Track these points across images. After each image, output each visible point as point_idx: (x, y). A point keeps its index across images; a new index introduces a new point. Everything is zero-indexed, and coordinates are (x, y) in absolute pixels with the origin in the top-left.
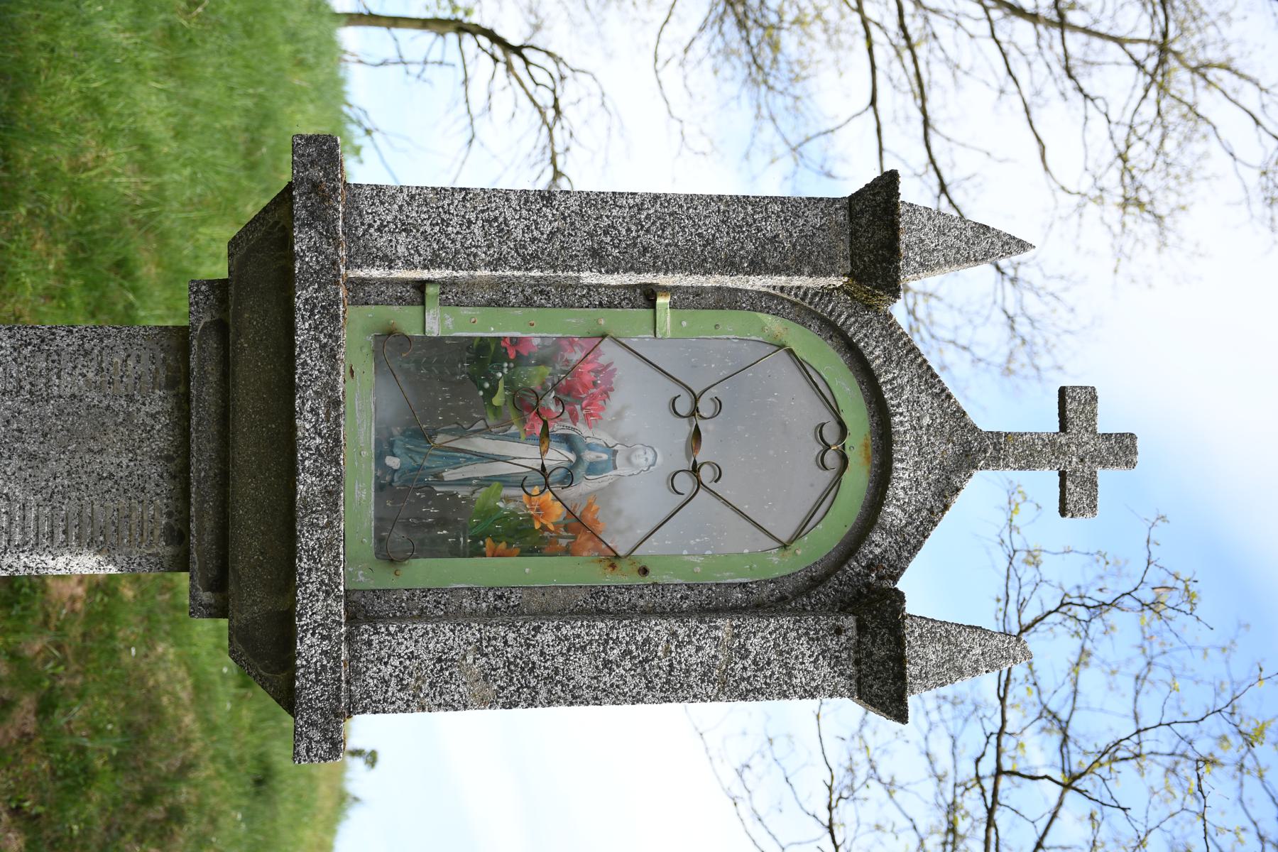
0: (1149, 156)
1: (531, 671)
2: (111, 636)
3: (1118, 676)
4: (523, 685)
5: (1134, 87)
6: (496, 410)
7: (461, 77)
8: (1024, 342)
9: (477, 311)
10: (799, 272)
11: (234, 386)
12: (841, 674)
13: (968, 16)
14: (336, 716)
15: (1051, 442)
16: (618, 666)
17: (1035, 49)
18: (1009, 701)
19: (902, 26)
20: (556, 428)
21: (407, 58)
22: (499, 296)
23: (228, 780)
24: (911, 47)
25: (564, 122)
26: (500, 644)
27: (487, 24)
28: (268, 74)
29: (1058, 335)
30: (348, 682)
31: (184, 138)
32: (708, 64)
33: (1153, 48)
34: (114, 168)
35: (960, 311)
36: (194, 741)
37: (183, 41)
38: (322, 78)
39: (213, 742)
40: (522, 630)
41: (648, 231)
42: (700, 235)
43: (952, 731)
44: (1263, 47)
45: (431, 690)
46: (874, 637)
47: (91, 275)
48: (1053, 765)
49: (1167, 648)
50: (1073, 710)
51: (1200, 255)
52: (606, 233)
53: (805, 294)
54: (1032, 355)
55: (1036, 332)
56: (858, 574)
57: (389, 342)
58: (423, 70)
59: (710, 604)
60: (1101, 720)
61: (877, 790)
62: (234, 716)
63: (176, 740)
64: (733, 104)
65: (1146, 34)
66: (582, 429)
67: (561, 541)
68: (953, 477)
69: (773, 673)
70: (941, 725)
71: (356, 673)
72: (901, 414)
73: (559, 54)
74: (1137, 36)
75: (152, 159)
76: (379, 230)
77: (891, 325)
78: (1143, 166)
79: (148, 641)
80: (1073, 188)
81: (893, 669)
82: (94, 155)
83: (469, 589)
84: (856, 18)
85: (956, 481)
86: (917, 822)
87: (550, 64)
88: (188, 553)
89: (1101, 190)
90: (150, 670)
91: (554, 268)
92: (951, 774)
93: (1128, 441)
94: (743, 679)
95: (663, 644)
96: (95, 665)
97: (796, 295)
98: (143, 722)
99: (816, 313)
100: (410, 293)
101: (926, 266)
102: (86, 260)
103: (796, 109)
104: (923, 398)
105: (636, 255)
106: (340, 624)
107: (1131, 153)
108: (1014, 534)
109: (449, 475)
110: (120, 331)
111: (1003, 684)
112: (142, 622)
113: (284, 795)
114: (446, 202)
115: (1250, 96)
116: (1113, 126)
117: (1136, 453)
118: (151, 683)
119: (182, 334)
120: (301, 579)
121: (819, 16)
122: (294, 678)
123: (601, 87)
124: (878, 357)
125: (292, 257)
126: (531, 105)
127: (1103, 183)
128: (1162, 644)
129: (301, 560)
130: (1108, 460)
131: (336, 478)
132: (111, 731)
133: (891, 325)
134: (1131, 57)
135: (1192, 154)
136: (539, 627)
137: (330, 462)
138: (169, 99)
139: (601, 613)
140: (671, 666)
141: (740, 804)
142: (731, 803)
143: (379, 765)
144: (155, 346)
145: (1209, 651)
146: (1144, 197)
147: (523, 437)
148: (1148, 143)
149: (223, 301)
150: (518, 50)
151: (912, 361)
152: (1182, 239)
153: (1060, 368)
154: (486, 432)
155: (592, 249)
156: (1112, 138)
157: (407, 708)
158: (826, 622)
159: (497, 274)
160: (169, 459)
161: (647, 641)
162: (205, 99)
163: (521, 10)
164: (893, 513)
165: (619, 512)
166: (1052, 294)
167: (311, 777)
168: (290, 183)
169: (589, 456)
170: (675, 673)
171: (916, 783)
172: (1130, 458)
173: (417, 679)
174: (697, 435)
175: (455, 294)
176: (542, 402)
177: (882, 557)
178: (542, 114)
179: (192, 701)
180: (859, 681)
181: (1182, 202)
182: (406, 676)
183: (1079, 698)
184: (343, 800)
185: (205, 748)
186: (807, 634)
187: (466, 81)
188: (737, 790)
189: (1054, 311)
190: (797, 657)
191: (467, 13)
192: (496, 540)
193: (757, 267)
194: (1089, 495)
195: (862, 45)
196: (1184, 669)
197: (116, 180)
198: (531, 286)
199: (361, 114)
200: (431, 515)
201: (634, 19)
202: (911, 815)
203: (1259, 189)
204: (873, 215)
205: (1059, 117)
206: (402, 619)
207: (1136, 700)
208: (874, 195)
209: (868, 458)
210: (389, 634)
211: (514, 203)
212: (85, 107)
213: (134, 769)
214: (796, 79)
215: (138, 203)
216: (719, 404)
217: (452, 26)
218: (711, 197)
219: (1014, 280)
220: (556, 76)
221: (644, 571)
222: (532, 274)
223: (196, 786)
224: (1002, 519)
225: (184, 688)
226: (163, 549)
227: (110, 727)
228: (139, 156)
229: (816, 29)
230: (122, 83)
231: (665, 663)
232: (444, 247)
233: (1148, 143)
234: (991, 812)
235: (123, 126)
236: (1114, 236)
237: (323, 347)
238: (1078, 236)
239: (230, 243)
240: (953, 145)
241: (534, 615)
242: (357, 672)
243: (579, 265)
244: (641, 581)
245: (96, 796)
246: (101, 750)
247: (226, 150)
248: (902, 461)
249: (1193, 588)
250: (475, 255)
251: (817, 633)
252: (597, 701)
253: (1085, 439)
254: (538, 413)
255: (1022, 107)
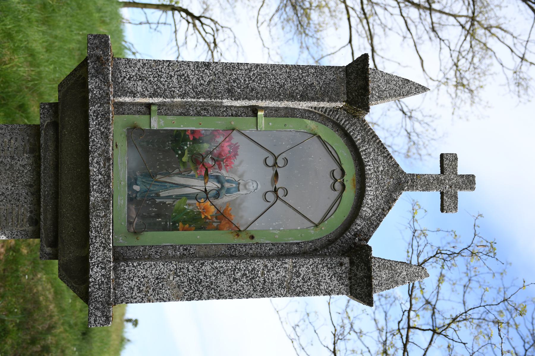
0: (467, 65)
1: (200, 283)
2: (17, 270)
3: (456, 285)
4: (196, 290)
5: (461, 35)
6: (184, 163)
7: (174, 29)
8: (414, 143)
9: (175, 118)
10: (323, 100)
11: (61, 152)
12: (343, 284)
13: (390, 6)
14: (108, 305)
15: (436, 178)
16: (240, 281)
17: (418, 20)
18: (413, 296)
19: (363, 9)
20: (211, 172)
21: (150, 21)
22: (185, 111)
23: (70, 333)
24: (366, 18)
25: (218, 49)
26: (185, 271)
27: (185, 7)
28: (89, 26)
29: (429, 141)
30: (114, 289)
31: (50, 52)
32: (279, 26)
33: (468, 19)
34: (18, 64)
35: (387, 130)
36: (54, 316)
37: (51, 9)
38: (113, 29)
39: (63, 317)
40: (196, 264)
41: (254, 81)
42: (278, 83)
43: (385, 310)
44: (515, 19)
45: (154, 293)
46: (358, 267)
47: (7, 111)
48: (428, 324)
49: (477, 273)
50: (437, 300)
51: (489, 107)
52: (234, 82)
53: (326, 110)
54: (418, 149)
55: (419, 139)
56: (350, 238)
57: (134, 131)
58: (157, 27)
59: (282, 252)
60: (449, 305)
61: (353, 335)
62: (73, 305)
63: (46, 316)
64: (291, 42)
65: (465, 13)
66: (224, 173)
67: (214, 224)
68: (393, 194)
69: (311, 284)
70: (380, 307)
71: (118, 285)
72: (369, 165)
73: (216, 20)
74: (461, 14)
75: (35, 60)
76: (129, 79)
77: (365, 125)
78: (465, 69)
79: (34, 272)
80: (435, 78)
81: (366, 282)
82: (9, 57)
83: (171, 246)
84: (343, 6)
85: (394, 196)
86: (371, 349)
87: (212, 25)
88: (39, 229)
89: (447, 79)
90: (35, 285)
91: (211, 98)
92: (385, 328)
93: (471, 178)
94: (297, 287)
95: (261, 270)
96: (9, 283)
97: (322, 111)
98: (31, 308)
99: (331, 119)
100: (144, 109)
101: (381, 98)
102: (5, 104)
103: (317, 43)
104: (380, 158)
105: (248, 92)
106: (110, 262)
107: (460, 64)
108: (415, 223)
109: (162, 194)
110: (8, 127)
111: (410, 289)
112: (31, 264)
113: (95, 339)
114: (160, 67)
115: (509, 40)
116: (452, 52)
117: (475, 184)
118: (35, 291)
119: (37, 129)
120: (92, 241)
121: (327, 5)
122: (88, 287)
123: (234, 34)
124: (359, 139)
125: (88, 91)
126: (204, 42)
127: (448, 76)
128: (475, 272)
129: (92, 232)
130: (462, 187)
131: (108, 194)
132: (16, 312)
133: (365, 125)
134: (459, 23)
135: (485, 64)
136: (204, 263)
137: (106, 187)
138: (43, 34)
139: (232, 257)
140: (265, 280)
141: (295, 342)
142: (291, 341)
143: (138, 326)
144: (24, 134)
145: (495, 274)
146: (465, 82)
147: (197, 176)
148: (467, 59)
149: (56, 113)
150: (198, 18)
151: (374, 141)
152: (481, 100)
153: (430, 155)
154: (180, 174)
155: (228, 89)
156: (451, 56)
157: (142, 301)
158: (336, 260)
159: (184, 100)
160: (31, 186)
161: (254, 269)
162: (60, 36)
163: (200, 3)
164: (366, 211)
165: (242, 217)
166: (426, 123)
167: (108, 331)
168: (87, 57)
169: (227, 185)
170: (267, 284)
171: (371, 332)
172: (472, 186)
173: (147, 287)
174: (276, 175)
175: (165, 110)
176: (205, 160)
177: (361, 231)
178: (209, 45)
179: (53, 298)
180: (350, 287)
181: (481, 84)
182: (142, 286)
183: (439, 295)
184: (123, 341)
185: (59, 319)
186: (327, 266)
187: (176, 32)
188: (293, 336)
189: (427, 130)
190: (322, 276)
191: (176, 3)
192: (184, 222)
193: (304, 98)
194: (454, 203)
195: (345, 17)
196: (485, 282)
197: (19, 69)
198: (200, 106)
199: (130, 45)
200: (154, 212)
201: (248, 6)
202: (368, 346)
203: (513, 79)
204: (357, 74)
205: (429, 49)
206: (140, 259)
207: (464, 296)
208: (357, 65)
209: (354, 186)
210: (134, 266)
211: (192, 68)
212: (4, 37)
213: (27, 329)
214: (317, 31)
215: (29, 79)
216: (286, 161)
217: (169, 8)
218: (283, 65)
219: (410, 117)
220: (215, 29)
221: (252, 237)
222: (200, 100)
223: (55, 336)
224: (410, 216)
225: (50, 293)
226: (28, 228)
227: (16, 310)
228: (30, 59)
229: (326, 10)
230: (21, 26)
231: (262, 279)
232: (159, 88)
233: (467, 59)
234: (405, 346)
235: (22, 45)
236: (453, 98)
237: (102, 133)
238: (437, 99)
239: (59, 86)
240: (384, 60)
241: (202, 257)
242: (118, 284)
243: (222, 96)
244: (251, 242)
245: (9, 341)
246: (12, 321)
247: (70, 58)
248: (370, 187)
249: (495, 246)
250: (174, 92)
251: (331, 265)
252: (231, 297)
253: (452, 177)
254: (203, 165)
255: (413, 44)
